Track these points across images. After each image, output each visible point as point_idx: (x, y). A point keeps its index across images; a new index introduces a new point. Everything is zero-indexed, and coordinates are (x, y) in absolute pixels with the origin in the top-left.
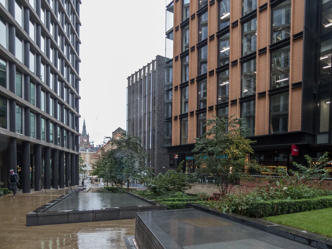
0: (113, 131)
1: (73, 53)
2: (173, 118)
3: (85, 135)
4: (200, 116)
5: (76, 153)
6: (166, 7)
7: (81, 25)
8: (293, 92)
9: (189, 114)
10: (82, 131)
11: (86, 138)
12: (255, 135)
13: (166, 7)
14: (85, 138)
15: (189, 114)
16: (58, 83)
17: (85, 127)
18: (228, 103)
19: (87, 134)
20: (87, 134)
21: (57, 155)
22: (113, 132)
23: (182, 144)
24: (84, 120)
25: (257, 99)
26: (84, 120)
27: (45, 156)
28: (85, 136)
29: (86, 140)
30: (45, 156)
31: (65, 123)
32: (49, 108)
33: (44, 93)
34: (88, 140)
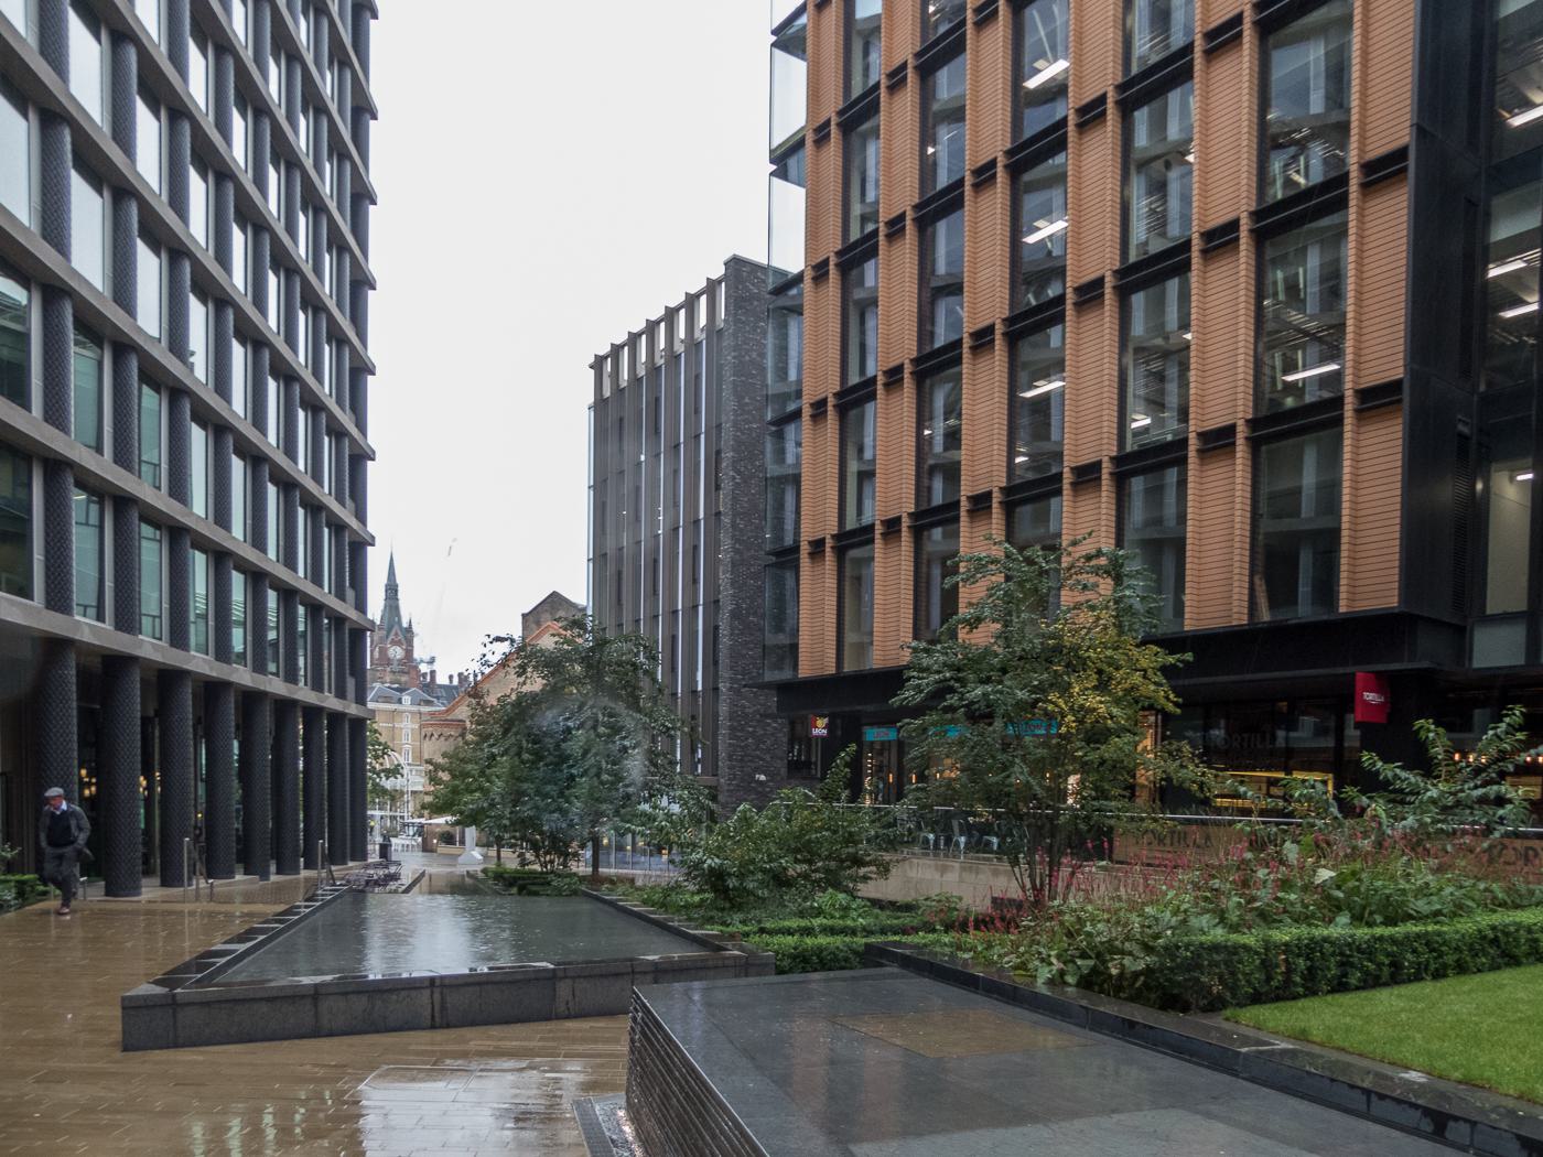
0: (527, 611)
1: (338, 245)
2: (805, 548)
3: (396, 627)
4: (929, 537)
5: (353, 709)
6: (774, 33)
7: (375, 117)
8: (1362, 430)
9: (879, 529)
10: (382, 607)
11: (398, 643)
12: (1186, 629)
13: (774, 33)
14: (394, 643)
15: (879, 529)
16: (272, 385)
17: (396, 591)
18: (1059, 476)
19: (405, 625)
20: (405, 625)
21: (266, 720)
22: (524, 616)
23: (848, 668)
24: (392, 560)
25: (1196, 460)
26: (392, 560)
27: (207, 726)
28: (396, 634)
29: (398, 649)
30: (207, 726)
31: (301, 573)
32: (230, 503)
33: (203, 433)
34: (409, 652)
